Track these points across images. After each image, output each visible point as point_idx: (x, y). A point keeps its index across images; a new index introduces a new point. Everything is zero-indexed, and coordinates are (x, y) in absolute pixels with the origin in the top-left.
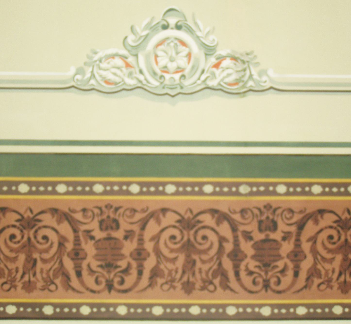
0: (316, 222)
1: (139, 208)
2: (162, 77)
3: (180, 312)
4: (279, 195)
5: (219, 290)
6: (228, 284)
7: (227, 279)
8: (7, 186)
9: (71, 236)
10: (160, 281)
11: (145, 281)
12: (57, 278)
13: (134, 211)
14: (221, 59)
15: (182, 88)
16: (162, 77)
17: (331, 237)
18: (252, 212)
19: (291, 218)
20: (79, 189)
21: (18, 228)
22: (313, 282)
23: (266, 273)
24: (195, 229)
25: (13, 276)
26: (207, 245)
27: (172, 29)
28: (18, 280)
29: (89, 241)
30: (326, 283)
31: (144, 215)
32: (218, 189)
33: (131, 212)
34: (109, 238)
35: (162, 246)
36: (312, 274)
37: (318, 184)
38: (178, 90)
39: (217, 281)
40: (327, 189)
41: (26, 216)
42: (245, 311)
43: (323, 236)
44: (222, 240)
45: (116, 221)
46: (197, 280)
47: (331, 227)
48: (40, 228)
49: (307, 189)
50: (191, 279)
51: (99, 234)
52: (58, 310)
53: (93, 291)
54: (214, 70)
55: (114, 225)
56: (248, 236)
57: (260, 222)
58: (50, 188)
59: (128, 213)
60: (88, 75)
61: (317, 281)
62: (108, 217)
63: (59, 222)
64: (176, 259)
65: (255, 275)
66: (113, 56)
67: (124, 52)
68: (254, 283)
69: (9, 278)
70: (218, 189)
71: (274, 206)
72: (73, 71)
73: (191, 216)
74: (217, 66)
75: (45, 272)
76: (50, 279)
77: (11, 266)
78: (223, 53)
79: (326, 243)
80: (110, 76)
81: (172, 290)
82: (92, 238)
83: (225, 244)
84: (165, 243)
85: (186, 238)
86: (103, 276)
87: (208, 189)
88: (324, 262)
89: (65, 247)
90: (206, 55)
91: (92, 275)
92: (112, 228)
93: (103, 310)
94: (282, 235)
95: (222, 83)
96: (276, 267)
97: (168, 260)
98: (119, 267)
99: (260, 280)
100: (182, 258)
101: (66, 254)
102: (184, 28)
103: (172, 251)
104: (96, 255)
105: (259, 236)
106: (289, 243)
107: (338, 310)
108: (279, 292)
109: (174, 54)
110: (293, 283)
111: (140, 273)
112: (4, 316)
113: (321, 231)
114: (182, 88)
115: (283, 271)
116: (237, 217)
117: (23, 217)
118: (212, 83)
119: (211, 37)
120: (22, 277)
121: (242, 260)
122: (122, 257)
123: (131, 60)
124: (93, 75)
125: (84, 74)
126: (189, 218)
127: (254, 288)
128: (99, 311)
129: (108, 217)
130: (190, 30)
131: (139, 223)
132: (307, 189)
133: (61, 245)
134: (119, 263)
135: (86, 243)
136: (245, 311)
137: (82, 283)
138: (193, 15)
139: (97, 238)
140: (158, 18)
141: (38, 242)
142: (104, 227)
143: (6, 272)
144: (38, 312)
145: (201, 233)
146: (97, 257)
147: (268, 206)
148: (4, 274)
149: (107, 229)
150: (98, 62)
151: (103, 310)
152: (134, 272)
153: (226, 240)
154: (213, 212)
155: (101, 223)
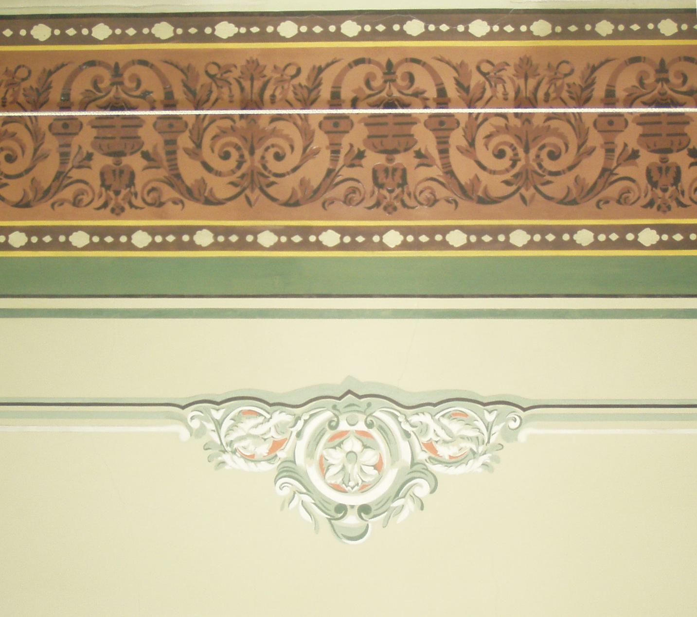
0: (303, 183)
1: (613, 205)
2: (370, 425)
3: (437, 24)
4: (21, 229)
10: (32, 82)
12: (478, 84)
13: (347, 201)
14: (271, 457)
15: (334, 407)
16: (370, 425)
20: (234, 238)
21: (270, 172)
22: (309, 78)
24: (517, 169)
25: (553, 87)
27: (352, 507)
29: (151, 151)
30: (285, 77)
31: (329, 195)
32: (96, 239)
34: (390, 152)
35: (299, 143)
38: (341, 404)
42: (325, 26)
43: (292, 159)
44: (195, 153)
46: (513, 81)
47: (282, 175)
49: (62, 239)
51: (135, 162)
53: (144, 63)
54: (279, 437)
55: (382, 178)
57: (404, 183)
60: (496, 429)
65: (138, 93)
66: (454, 461)
67: (437, 468)
68: (411, 78)
70: (96, 239)
72: (523, 435)
73: (523, 191)
74: (277, 445)
76: (216, 83)
78: (264, 466)
79: (19, 151)
80: (455, 427)
82: (146, 156)
83: (464, 143)
90: (294, 462)
92: (386, 170)
93: (635, 27)
94: (364, 162)
95: (268, 416)
99: (675, 81)
101: (190, 126)
102: (332, 508)
107: (41, 32)
108: (92, 64)
109: (349, 467)
110: (615, 76)
112: (52, 21)
113: (570, 168)
114: (334, 407)
117: (262, 190)
118: (281, 417)
119: (287, 491)
120: (539, 84)
123: (422, 456)
124: (489, 427)
125: (507, 429)
127: (139, 70)
128: (139, 30)
130: (322, 503)
132: (473, 239)
135: (155, 147)
137: (164, 80)
138: (317, 528)
139: (138, 155)
140: (374, 523)
141: (511, 146)
150: (481, 449)
153: (186, 150)
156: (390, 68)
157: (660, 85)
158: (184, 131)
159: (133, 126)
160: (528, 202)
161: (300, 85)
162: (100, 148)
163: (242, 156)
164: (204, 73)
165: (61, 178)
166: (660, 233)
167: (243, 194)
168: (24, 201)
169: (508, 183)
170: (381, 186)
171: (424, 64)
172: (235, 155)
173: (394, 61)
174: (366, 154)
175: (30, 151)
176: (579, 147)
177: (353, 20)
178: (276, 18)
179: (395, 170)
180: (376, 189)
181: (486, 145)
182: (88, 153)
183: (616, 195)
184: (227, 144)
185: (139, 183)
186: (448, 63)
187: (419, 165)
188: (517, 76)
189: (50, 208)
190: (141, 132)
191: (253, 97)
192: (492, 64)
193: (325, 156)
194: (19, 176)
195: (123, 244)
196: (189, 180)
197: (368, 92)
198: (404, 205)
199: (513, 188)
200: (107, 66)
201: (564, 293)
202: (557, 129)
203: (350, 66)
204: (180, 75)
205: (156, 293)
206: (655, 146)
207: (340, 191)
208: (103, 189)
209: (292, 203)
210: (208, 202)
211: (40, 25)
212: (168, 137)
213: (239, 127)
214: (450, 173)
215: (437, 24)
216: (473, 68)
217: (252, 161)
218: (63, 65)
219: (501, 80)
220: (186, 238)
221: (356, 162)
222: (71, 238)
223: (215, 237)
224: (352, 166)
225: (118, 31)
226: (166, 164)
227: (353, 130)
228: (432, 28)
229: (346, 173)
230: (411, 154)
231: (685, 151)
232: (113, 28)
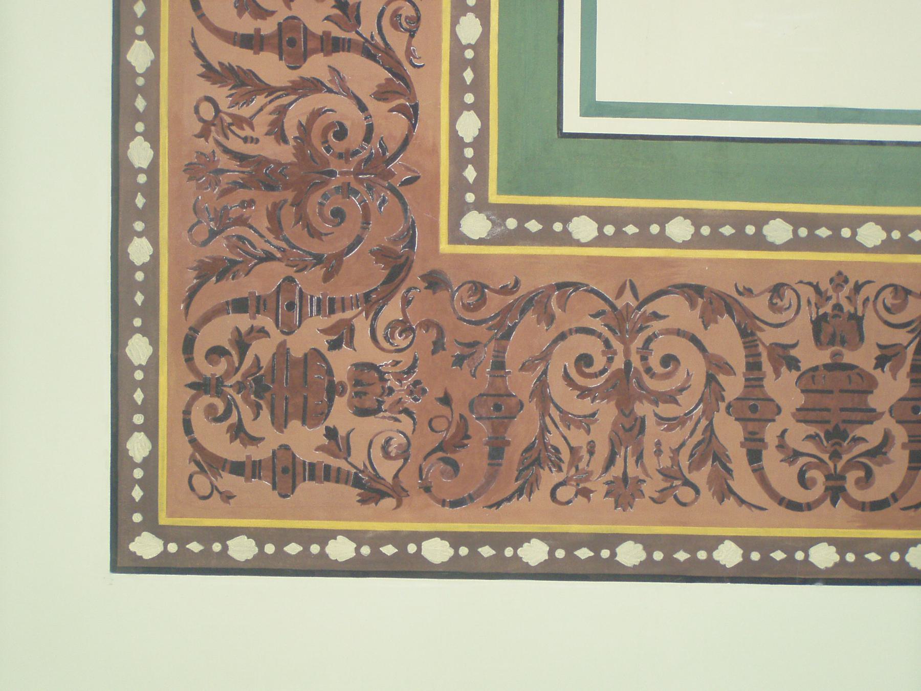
3: (693, 560)
6: (730, 482)
9: (737, 357)
19: (901, 308)
23: (836, 455)
29: (784, 369)
34: (836, 366)
39: (700, 477)
49: (655, 229)
50: (633, 471)
52: (366, 550)
62: (838, 307)
65: (802, 461)
77: (578, 438)
81: (581, 499)
82: (793, 364)
85: (619, 363)
87: (778, 231)
92: (843, 343)
94: (877, 352)
97: (568, 420)
100: (607, 412)
103: (584, 392)
106: (894, 375)
116: (759, 306)
132: (803, 232)
136: (766, 558)
147: (840, 279)
153: (729, 370)
155: (818, 324)
159: (813, 410)
162: (863, 375)
163: (644, 358)
164: (701, 491)
167: (641, 299)
169: (656, 316)
171: (781, 501)
172: (654, 361)
174: (873, 362)
178: (738, 575)
179: (832, 342)
184: (668, 376)
186: (742, 501)
187: (794, 346)
189: (523, 279)
190: (800, 400)
198: (816, 288)
201: (842, 146)
205: (875, 147)
206: (849, 377)
208: (860, 313)
210: (699, 290)
212: (757, 393)
214: (747, 334)
215: (693, 560)
216: (706, 494)
217: (627, 353)
219: (665, 474)
220: (846, 233)
221: (888, 352)
222: (883, 235)
224: (473, 345)
225: (702, 555)
226: (761, 348)
227: (775, 399)
228: (800, 556)
229: (481, 333)
230: (333, 357)
231: (804, 366)
232: (710, 560)
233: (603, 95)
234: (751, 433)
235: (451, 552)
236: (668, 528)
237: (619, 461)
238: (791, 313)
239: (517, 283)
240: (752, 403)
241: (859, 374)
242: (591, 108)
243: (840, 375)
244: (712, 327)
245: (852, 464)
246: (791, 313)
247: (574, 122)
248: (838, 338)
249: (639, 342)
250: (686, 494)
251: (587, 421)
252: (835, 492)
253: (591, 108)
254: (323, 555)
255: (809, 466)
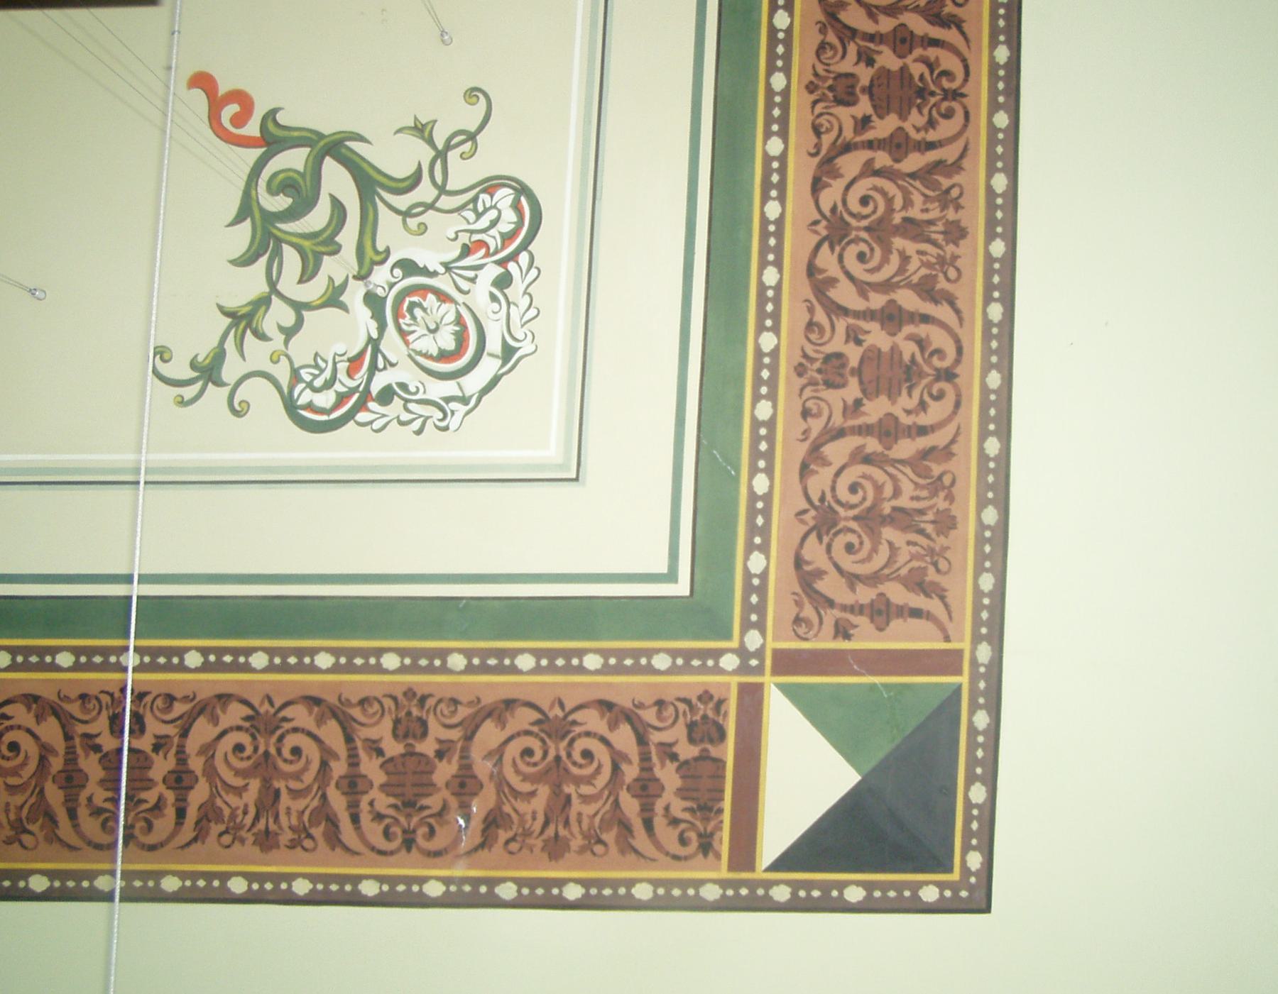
0: (502, 723)
5: (951, 465)
7: (933, 449)
8: (765, 319)
9: (851, 442)
11: (943, 312)
17: (849, 548)
18: (821, 115)
23: (933, 94)
25: (923, 552)
26: (869, 486)
28: (931, 544)
29: (668, 762)
33: (813, 331)
36: (938, 16)
37: (760, 274)
40: (778, 99)
41: (824, 233)
42: (994, 420)
43: (514, 749)
45: (828, 358)
48: (834, 497)
50: (940, 227)
56: (864, 123)
58: (763, 431)
59: (813, 337)
61: (942, 284)
62: (819, 371)
63: (836, 175)
64: (890, 544)
65: (926, 398)
69: (928, 559)
71: (810, 77)
75: (918, 493)
79: (519, 761)
84: (871, 271)
86: (929, 386)
88: (906, 271)
89: (874, 453)
91: (937, 123)
94: (862, 65)
96: (922, 77)
98: (913, 356)
100: (888, 533)
104: (890, 397)
105: (864, 106)
111: (926, 319)
113: (223, 734)
115: (931, 66)
120: (928, 537)
121: (907, 136)
122: (904, 69)
126: (826, 228)
128: (194, 885)
129: (819, 371)
131: (834, 318)
133: (868, 460)
134: (906, 357)
135: (663, 765)
136: (994, 420)
139: (682, 757)
142: (838, 380)
143: (915, 564)
144: (1004, 199)
145: (854, 206)
146: (892, 396)
147: (800, 370)
148: (919, 568)
149: (853, 94)
151: (996, 279)
152: (923, 330)
154: (805, 470)
156: (409, 843)
157: (709, 829)
158: (341, 777)
159: (392, 785)
160: (557, 701)
161: (506, 830)
165: (471, 730)
166: (247, 663)
168: (223, 700)
170: (420, 719)
173: (404, 852)
175: (219, 756)
176: (213, 756)
177: (234, 893)
180: (424, 717)
181: (26, 757)
182: (157, 753)
183: (177, 705)
185: (387, 723)
187: (844, 402)
188: (567, 839)
190: (883, 399)
191: (265, 814)
192: (303, 848)
193: (476, 754)
194: (519, 734)
195: (20, 653)
196: (625, 731)
197: (432, 821)
199: (571, 718)
200: (419, 849)
202: (524, 780)
203: (162, 845)
204: (60, 833)
207: (179, 709)
209: (224, 699)
211: (171, 891)
213: (571, 785)
218: (182, 847)
221: (852, 335)
223: (77, 658)
233: (663, 569)
234: (915, 147)
235: (992, 455)
236: (976, 345)
237: (934, 236)
238: (823, 404)
239: (806, 301)
240: (898, 42)
241: (878, 79)
242: (671, 576)
243: (875, 90)
244: (841, 171)
245: (936, 82)
246: (823, 404)
247: (681, 588)
248: (850, 90)
249: (853, 222)
250: (955, 193)
251: (905, 259)
252: (956, 95)
253: (671, 576)
254: (1003, 195)
255: (931, 395)
